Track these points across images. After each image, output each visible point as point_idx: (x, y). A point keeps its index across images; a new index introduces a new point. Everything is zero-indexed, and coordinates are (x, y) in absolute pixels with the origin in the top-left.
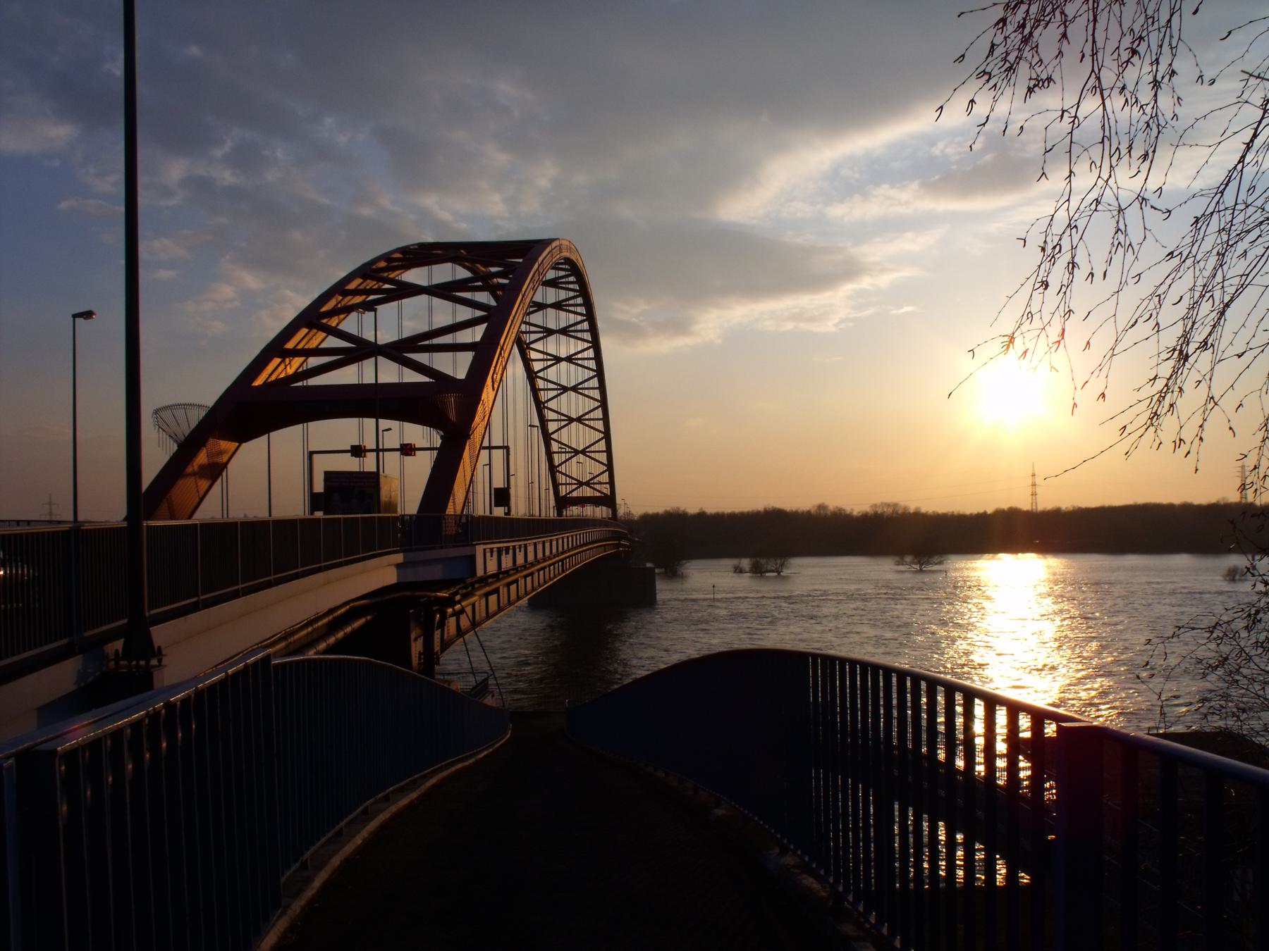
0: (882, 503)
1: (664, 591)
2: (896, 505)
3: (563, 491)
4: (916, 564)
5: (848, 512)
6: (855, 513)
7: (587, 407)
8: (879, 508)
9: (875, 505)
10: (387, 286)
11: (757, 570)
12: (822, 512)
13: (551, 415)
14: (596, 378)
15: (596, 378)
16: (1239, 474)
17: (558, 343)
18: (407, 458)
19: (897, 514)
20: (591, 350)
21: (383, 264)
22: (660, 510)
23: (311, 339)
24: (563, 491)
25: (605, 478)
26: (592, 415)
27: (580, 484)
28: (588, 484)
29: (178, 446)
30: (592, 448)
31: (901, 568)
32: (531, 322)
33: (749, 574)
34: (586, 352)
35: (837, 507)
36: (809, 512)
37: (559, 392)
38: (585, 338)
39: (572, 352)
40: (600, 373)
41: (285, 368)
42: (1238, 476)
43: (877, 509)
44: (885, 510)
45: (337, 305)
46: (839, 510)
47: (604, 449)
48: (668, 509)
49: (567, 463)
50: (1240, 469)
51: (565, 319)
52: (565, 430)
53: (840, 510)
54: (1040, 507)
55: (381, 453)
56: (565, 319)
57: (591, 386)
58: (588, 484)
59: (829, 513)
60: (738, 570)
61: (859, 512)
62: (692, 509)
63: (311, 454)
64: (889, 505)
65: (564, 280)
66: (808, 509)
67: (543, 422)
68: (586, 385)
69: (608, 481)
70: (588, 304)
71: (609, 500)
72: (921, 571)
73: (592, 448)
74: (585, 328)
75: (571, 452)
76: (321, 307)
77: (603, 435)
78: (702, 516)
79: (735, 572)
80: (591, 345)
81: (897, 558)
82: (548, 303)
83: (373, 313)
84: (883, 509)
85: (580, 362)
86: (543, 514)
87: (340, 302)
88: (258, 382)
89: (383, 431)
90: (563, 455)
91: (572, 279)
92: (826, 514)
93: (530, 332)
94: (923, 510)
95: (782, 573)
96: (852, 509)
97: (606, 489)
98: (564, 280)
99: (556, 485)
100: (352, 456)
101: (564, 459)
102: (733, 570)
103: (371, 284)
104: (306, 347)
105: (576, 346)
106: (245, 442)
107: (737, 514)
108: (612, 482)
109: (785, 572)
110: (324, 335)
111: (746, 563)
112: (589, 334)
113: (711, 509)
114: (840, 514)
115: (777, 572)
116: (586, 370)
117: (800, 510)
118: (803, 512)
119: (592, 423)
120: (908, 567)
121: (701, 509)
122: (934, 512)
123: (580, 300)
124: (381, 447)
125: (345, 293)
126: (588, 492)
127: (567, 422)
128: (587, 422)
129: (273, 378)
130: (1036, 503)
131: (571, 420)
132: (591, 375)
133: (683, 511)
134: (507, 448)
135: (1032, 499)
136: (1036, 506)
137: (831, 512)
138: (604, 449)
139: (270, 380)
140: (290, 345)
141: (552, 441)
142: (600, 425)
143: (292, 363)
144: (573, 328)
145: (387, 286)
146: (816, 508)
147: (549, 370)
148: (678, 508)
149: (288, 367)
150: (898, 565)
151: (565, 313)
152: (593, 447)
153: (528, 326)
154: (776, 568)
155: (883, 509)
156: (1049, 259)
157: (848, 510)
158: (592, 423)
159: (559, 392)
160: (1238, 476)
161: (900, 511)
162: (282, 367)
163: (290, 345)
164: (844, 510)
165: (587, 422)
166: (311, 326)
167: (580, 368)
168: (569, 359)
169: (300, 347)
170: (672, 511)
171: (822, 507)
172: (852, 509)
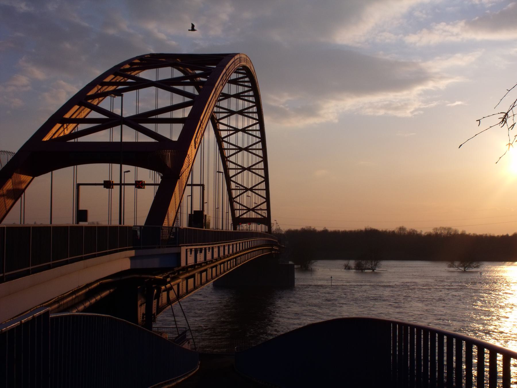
0: (440, 227)
2: (449, 229)
3: (237, 214)
4: (462, 267)
6: (423, 233)
8: (439, 230)
9: (436, 229)
10: (129, 80)
11: (359, 268)
12: (402, 232)
13: (231, 166)
14: (263, 162)
15: (263, 162)
17: (237, 120)
18: (139, 190)
20: (258, 125)
21: (127, 66)
22: (299, 228)
23: (81, 112)
24: (237, 214)
25: (264, 206)
26: (257, 166)
27: (249, 210)
28: (253, 210)
29: (161, 178)
30: (257, 187)
31: (452, 269)
33: (354, 270)
34: (254, 126)
36: (393, 232)
37: (237, 151)
38: (254, 117)
39: (250, 165)
40: (265, 159)
41: (64, 130)
43: (437, 231)
44: (443, 232)
45: (98, 91)
46: (413, 231)
47: (265, 188)
48: (304, 227)
49: (241, 196)
51: (241, 104)
53: (414, 231)
55: (123, 186)
56: (241, 104)
57: (257, 148)
58: (253, 210)
59: (406, 233)
60: (348, 268)
62: (319, 228)
63: (78, 185)
64: (445, 229)
65: (242, 80)
66: (393, 230)
67: (226, 169)
68: (254, 147)
70: (257, 96)
71: (266, 221)
72: (465, 271)
73: (257, 187)
74: (255, 111)
75: (243, 189)
76: (88, 93)
77: (264, 179)
78: (325, 232)
79: (345, 269)
80: (258, 121)
81: (450, 263)
83: (121, 97)
84: (441, 231)
86: (224, 228)
87: (100, 89)
88: (46, 139)
89: (124, 172)
90: (238, 191)
91: (247, 79)
92: (405, 233)
95: (375, 271)
96: (421, 231)
97: (265, 214)
98: (242, 80)
99: (233, 210)
100: (104, 187)
101: (238, 194)
102: (344, 267)
103: (119, 79)
104: (78, 117)
105: (248, 121)
106: (37, 176)
108: (268, 209)
109: (377, 270)
110: (89, 110)
111: (352, 263)
113: (331, 229)
114: (414, 233)
115: (372, 269)
116: (257, 157)
118: (390, 232)
119: (257, 171)
121: (325, 228)
122: (474, 234)
123: (251, 93)
124: (123, 182)
125: (103, 84)
126: (253, 215)
127: (241, 170)
129: (56, 136)
131: (244, 169)
132: (257, 141)
134: (188, 196)
138: (265, 188)
139: (53, 138)
140: (67, 116)
141: (231, 182)
143: (68, 127)
145: (129, 80)
146: (398, 229)
147: (238, 175)
148: (310, 227)
149: (66, 130)
150: (450, 267)
152: (257, 187)
154: (372, 267)
155: (441, 231)
157: (419, 231)
158: (257, 171)
159: (237, 151)
161: (452, 233)
162: (62, 129)
163: (67, 116)
164: (416, 231)
166: (81, 104)
168: (244, 130)
169: (73, 117)
170: (306, 229)
171: (402, 229)
172: (421, 231)
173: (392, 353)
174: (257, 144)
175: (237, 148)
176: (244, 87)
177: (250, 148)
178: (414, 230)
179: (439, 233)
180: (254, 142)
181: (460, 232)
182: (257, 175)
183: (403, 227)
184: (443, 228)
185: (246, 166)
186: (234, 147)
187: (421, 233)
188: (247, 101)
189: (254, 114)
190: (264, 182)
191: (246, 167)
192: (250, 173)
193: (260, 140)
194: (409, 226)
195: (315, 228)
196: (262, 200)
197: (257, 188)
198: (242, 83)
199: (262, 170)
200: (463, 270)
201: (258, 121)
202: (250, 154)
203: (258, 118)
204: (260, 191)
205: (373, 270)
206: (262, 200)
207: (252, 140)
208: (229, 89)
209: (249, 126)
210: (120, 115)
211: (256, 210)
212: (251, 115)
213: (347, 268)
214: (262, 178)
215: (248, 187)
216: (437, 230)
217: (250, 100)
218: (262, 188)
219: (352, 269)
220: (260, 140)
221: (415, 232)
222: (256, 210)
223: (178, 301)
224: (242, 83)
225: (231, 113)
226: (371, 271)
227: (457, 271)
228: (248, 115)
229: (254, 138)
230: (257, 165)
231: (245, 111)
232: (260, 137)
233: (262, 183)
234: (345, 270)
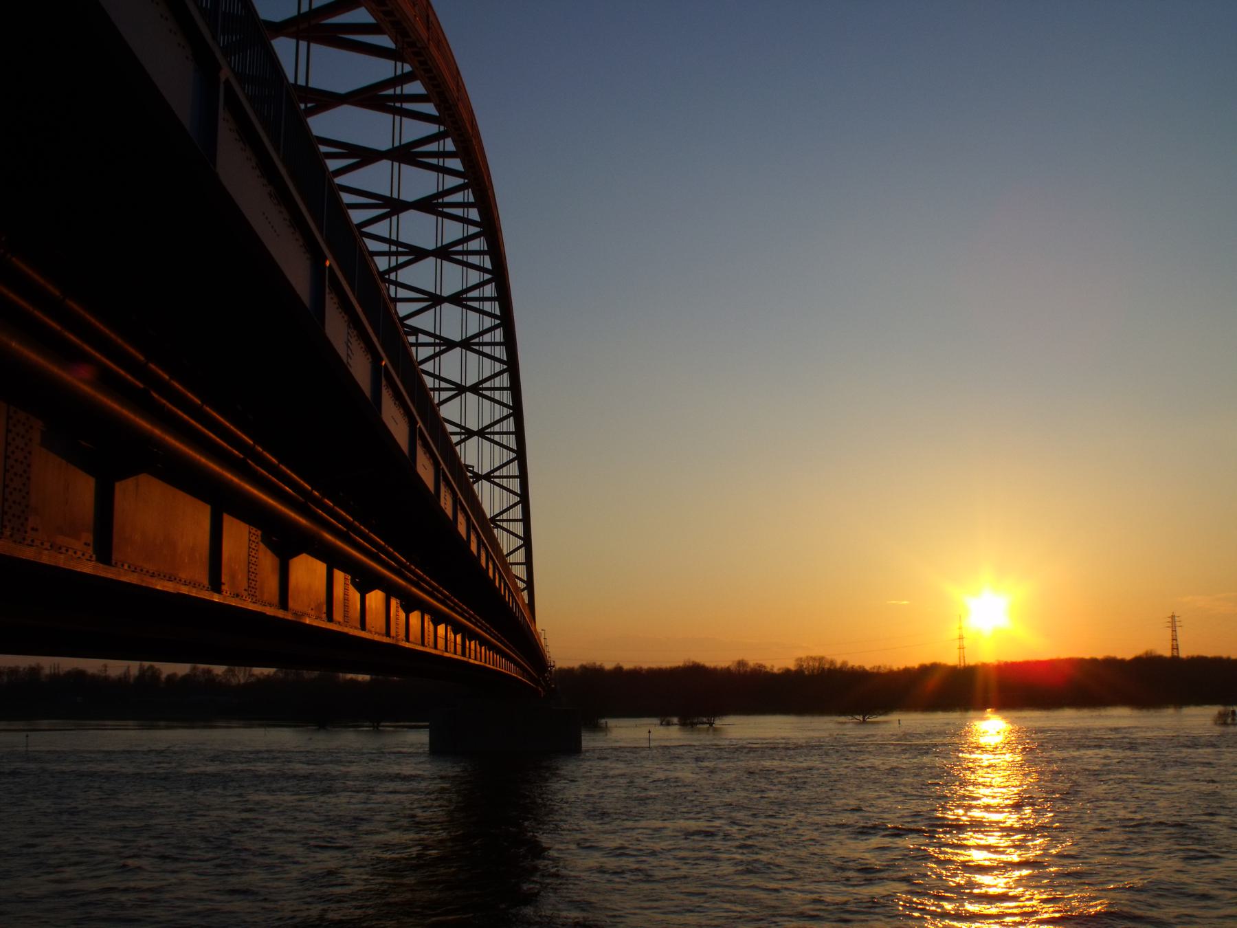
0: (807, 657)
1: (589, 741)
2: (821, 659)
5: (768, 670)
6: (775, 670)
7: (511, 547)
9: (800, 659)
12: (741, 669)
14: (512, 418)
15: (512, 418)
16: (1170, 625)
19: (823, 669)
20: (506, 375)
22: (576, 664)
26: (505, 471)
30: (505, 516)
32: (400, 240)
33: (677, 727)
34: (497, 379)
35: (757, 664)
36: (728, 669)
37: (437, 349)
38: (497, 355)
39: (487, 422)
40: (520, 455)
42: (1168, 627)
43: (803, 663)
44: (811, 664)
48: (584, 663)
50: (1170, 620)
52: (487, 374)
53: (761, 666)
54: (1184, 653)
56: (453, 278)
57: (505, 430)
59: (748, 669)
61: (779, 669)
62: (609, 666)
64: (814, 659)
69: (521, 517)
70: (496, 250)
73: (505, 516)
74: (497, 340)
77: (515, 455)
78: (618, 670)
80: (505, 367)
82: (458, 349)
85: (497, 438)
91: (449, 145)
93: (440, 389)
94: (851, 664)
95: (714, 725)
96: (773, 666)
107: (656, 669)
111: (675, 720)
112: (487, 258)
113: (627, 666)
115: (708, 723)
116: (505, 450)
117: (719, 667)
118: (722, 668)
119: (505, 482)
120: (850, 718)
121: (618, 664)
122: (860, 667)
128: (497, 480)
130: (964, 657)
132: (505, 414)
133: (852, 667)
135: (960, 653)
136: (964, 660)
137: (752, 669)
138: (517, 473)
142: (515, 485)
144: (476, 340)
146: (735, 664)
151: (458, 268)
153: (437, 381)
156: (270, 905)
158: (505, 482)
159: (437, 349)
160: (1168, 627)
161: (827, 666)
165: (497, 480)
167: (497, 447)
168: (466, 344)
171: (741, 663)
172: (773, 666)
173: (367, 677)
174: (505, 422)
175: (437, 341)
176: (466, 225)
177: (489, 430)
178: (762, 665)
179: (804, 666)
180: (497, 418)
181: (838, 665)
182: (505, 490)
183: (743, 660)
184: (811, 657)
185: (473, 425)
186: (431, 340)
187: (772, 669)
188: (471, 220)
189: (497, 348)
190: (516, 461)
191: (468, 393)
192: (486, 444)
193: (511, 411)
194: (753, 660)
195: (602, 664)
196: (511, 485)
197: (505, 518)
198: (400, 249)
199: (511, 436)
200: (862, 719)
201: (505, 367)
202: (487, 403)
203: (505, 359)
204: (505, 436)
205: (711, 724)
206: (511, 485)
207: (489, 367)
208: (439, 277)
209: (464, 190)
210: (398, 288)
211: (489, 433)
212: (487, 350)
213: (664, 723)
214: (511, 453)
215: (463, 384)
216: (801, 662)
217: (485, 266)
218: (511, 474)
219: (672, 724)
220: (511, 411)
221: (763, 669)
222: (489, 433)
223: (30, 749)
224: (400, 249)
225: (435, 300)
226: (708, 725)
227: (852, 722)
228: (481, 350)
229: (497, 406)
230: (505, 468)
231: (446, 210)
232: (511, 405)
233: (511, 464)
234: (662, 727)
